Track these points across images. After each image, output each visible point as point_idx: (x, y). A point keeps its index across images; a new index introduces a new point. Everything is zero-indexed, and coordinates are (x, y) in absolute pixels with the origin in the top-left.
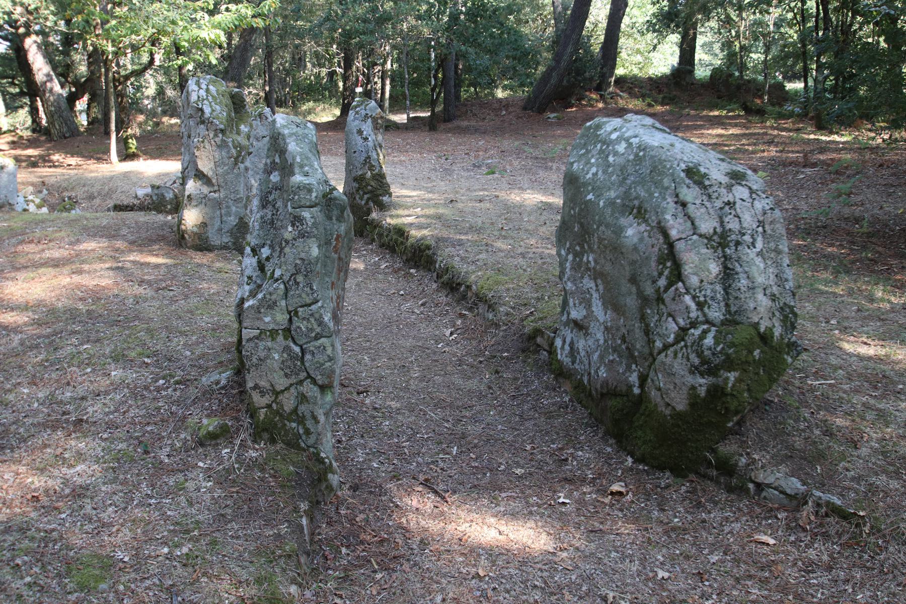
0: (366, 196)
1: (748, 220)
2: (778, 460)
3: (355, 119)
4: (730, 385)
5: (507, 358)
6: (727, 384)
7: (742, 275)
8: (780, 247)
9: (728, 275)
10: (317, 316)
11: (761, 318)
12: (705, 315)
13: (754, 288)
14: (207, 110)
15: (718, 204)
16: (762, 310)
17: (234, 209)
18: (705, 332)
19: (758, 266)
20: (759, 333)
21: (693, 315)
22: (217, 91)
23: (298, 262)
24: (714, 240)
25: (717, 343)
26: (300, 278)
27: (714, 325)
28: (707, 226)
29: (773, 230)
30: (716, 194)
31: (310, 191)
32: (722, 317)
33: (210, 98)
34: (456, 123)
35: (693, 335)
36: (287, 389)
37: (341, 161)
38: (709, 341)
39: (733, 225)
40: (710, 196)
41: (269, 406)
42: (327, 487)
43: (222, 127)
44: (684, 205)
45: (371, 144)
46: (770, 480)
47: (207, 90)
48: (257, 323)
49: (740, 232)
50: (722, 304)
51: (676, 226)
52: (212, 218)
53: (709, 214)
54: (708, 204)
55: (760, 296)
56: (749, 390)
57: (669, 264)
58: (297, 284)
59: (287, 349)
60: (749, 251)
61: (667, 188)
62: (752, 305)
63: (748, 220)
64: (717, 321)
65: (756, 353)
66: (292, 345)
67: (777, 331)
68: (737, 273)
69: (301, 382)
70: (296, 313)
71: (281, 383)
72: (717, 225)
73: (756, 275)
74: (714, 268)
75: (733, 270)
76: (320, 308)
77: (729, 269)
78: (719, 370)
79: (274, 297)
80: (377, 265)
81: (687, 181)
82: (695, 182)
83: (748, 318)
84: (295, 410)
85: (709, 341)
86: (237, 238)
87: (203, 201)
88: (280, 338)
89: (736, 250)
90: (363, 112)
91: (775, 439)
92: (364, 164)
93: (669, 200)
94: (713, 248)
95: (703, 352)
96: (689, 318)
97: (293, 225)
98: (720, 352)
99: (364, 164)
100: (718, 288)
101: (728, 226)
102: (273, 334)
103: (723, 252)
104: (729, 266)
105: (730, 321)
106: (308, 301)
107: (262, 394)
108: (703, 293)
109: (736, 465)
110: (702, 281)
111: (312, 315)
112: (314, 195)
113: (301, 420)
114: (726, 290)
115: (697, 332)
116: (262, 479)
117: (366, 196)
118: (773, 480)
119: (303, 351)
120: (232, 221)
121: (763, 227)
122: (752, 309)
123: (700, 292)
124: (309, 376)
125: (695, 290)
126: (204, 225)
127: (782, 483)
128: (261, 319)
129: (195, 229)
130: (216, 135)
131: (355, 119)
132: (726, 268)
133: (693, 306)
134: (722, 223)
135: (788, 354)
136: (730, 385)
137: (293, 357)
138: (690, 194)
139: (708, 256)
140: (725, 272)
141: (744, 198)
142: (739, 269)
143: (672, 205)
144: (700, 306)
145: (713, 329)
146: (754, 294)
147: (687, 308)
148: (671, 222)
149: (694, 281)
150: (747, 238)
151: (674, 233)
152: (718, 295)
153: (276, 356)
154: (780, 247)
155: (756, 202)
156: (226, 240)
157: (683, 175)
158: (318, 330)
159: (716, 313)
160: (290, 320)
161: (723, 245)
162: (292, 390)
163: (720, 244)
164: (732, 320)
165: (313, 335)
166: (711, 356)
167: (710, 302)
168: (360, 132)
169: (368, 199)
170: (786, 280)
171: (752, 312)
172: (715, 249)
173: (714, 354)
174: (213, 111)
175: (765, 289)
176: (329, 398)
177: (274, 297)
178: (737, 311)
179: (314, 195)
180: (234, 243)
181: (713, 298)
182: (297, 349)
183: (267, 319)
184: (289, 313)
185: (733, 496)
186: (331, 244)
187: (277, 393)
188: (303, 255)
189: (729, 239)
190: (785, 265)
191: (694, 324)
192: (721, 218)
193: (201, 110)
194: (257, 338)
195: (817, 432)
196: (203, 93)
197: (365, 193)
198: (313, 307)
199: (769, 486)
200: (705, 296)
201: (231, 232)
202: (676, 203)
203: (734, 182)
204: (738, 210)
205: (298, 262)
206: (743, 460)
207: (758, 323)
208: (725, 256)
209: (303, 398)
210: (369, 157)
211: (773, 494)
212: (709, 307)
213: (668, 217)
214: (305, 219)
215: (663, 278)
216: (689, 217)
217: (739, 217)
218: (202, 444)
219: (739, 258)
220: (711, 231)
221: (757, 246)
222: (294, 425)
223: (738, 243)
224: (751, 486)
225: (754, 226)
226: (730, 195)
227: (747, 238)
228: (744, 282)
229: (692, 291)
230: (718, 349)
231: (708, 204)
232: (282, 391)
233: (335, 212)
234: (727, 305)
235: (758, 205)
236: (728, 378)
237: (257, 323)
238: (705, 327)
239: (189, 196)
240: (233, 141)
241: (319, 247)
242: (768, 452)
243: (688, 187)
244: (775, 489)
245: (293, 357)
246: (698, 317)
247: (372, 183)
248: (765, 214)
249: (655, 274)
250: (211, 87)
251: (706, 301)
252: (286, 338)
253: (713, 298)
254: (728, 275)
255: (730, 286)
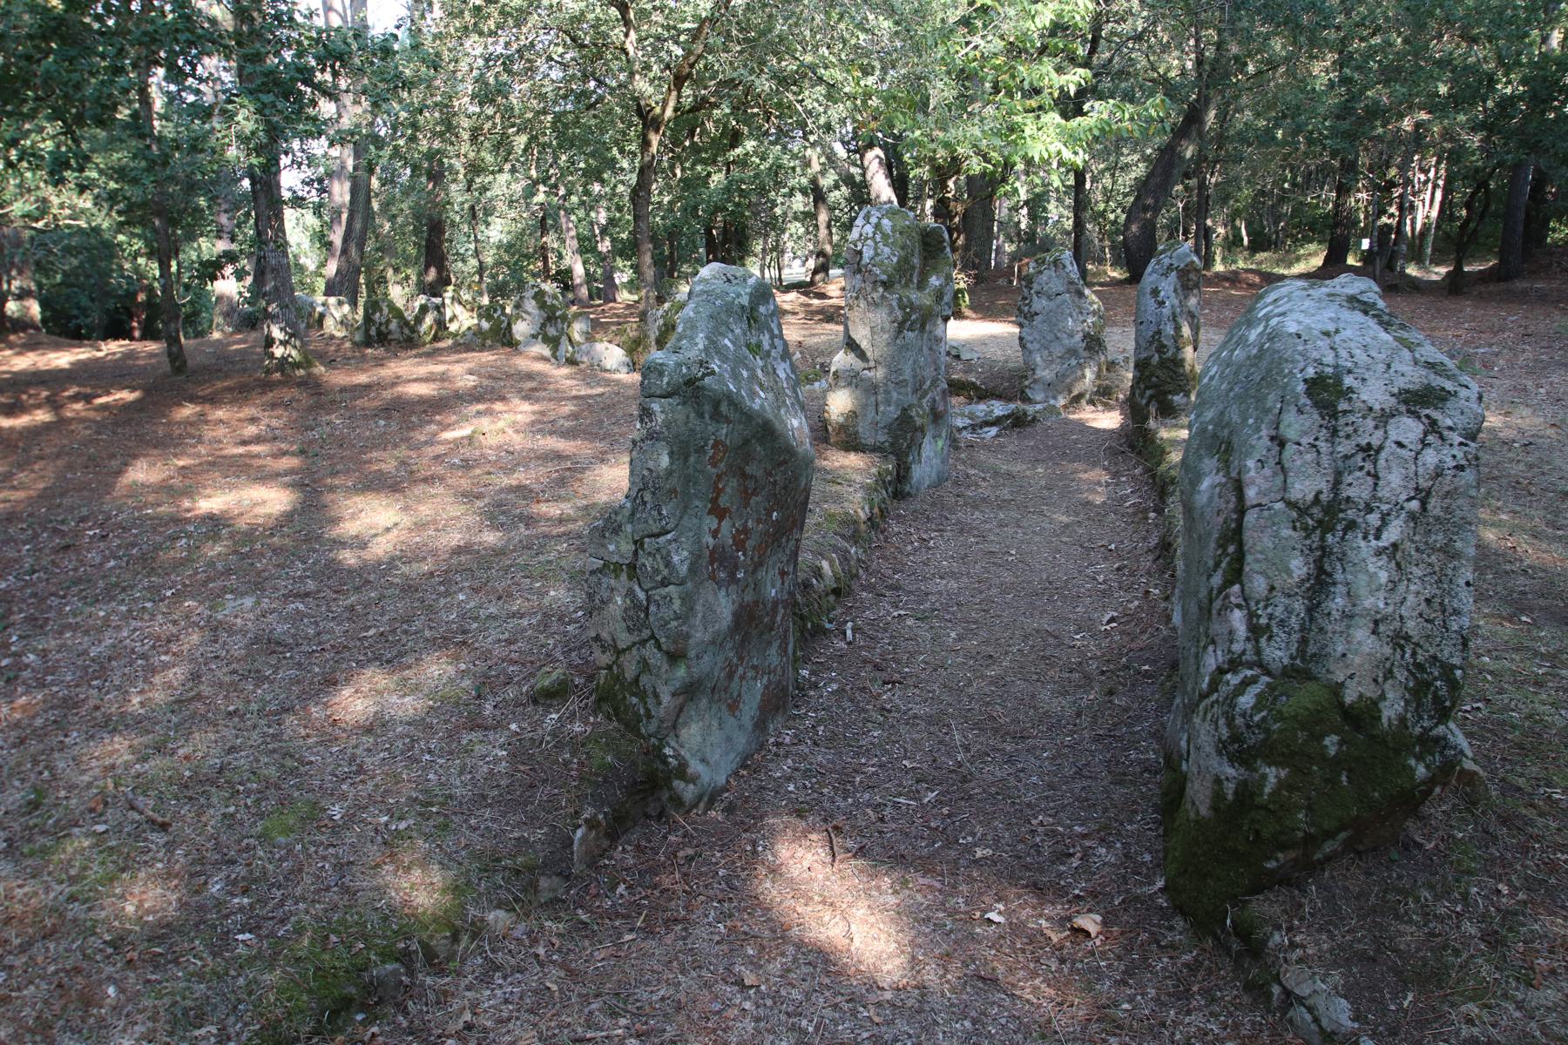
0: (1148, 392)
1: (1394, 481)
2: (1342, 958)
3: (1154, 271)
4: (1267, 790)
5: (1146, 674)
6: (1262, 787)
7: (1341, 589)
8: (1459, 545)
9: (1320, 583)
10: (664, 552)
11: (1351, 677)
12: (1258, 652)
13: (1351, 617)
14: (868, 253)
15: (1345, 447)
16: (1357, 660)
17: (895, 395)
18: (1246, 683)
19: (1373, 576)
20: (1341, 704)
21: (1237, 648)
22: (893, 227)
23: (646, 473)
24: (1311, 516)
25: (1257, 707)
26: (648, 497)
27: (1268, 673)
28: (1304, 487)
29: (1447, 510)
30: (1350, 429)
31: (661, 374)
32: (1286, 661)
33: (878, 238)
34: (1520, 285)
35: (1228, 683)
36: (629, 648)
37: (1131, 331)
38: (1246, 700)
39: (1357, 488)
40: (1334, 432)
41: (609, 668)
42: (671, 798)
43: (884, 277)
44: (1281, 443)
45: (1166, 311)
46: (1304, 990)
47: (878, 226)
48: (602, 552)
49: (1367, 505)
50: (1295, 637)
51: (1258, 481)
52: (865, 406)
53: (1318, 464)
54: (1323, 446)
55: (1361, 634)
56: (1309, 808)
57: (1231, 549)
58: (645, 503)
59: (630, 593)
60: (1363, 544)
61: (1268, 411)
62: (1340, 649)
63: (1394, 481)
64: (1275, 667)
65: (1331, 742)
66: (637, 588)
67: (1392, 709)
68: (1334, 584)
69: (643, 642)
70: (642, 544)
71: (624, 639)
72: (1324, 486)
73: (1363, 592)
74: (1299, 567)
75: (1330, 575)
76: (669, 542)
77: (1325, 572)
78: (1255, 757)
79: (619, 518)
80: (1124, 499)
81: (1304, 400)
82: (1316, 405)
83: (1328, 671)
84: (636, 680)
85: (1246, 700)
86: (896, 437)
87: (851, 379)
88: (624, 577)
89: (1343, 538)
90: (1167, 261)
91: (1361, 917)
92: (1151, 343)
93: (1264, 433)
94: (1305, 529)
95: (1233, 719)
96: (1230, 651)
97: (642, 421)
98: (1258, 726)
99: (1151, 343)
100: (1299, 606)
101: (1351, 492)
102: (617, 569)
103: (1322, 539)
104: (1327, 568)
105: (1297, 671)
106: (656, 531)
107: (604, 649)
108: (1269, 610)
109: (1264, 942)
110: (1272, 588)
111: (658, 550)
112: (666, 380)
113: (642, 695)
114: (1310, 610)
115: (1233, 679)
116: (566, 763)
117: (1148, 392)
118: (1308, 992)
119: (648, 598)
120: (893, 412)
121: (1424, 504)
122: (1338, 655)
123: (1266, 607)
124: (653, 637)
125: (1257, 603)
126: (853, 415)
127: (1320, 1002)
128: (604, 546)
129: (841, 420)
130: (875, 289)
131: (1154, 271)
132: (1321, 570)
133: (1241, 629)
134: (1336, 484)
135: (1419, 758)
136: (1267, 790)
137: (636, 605)
138: (1299, 424)
139: (1292, 543)
140: (1317, 577)
141: (1405, 442)
142: (1339, 576)
143: (1266, 441)
144: (1256, 631)
145: (1266, 679)
146: (1349, 627)
147: (1231, 632)
148: (1252, 473)
149: (1259, 585)
150: (1374, 519)
151: (1251, 493)
152: (1293, 619)
153: (619, 600)
154: (1459, 545)
155: (1429, 452)
156: (882, 439)
157: (1301, 387)
158: (665, 572)
159: (1277, 653)
160: (636, 553)
161: (1325, 527)
162: (634, 651)
163: (1320, 522)
164: (1300, 671)
165: (659, 578)
166: (1243, 729)
167: (1275, 630)
168: (1155, 292)
169: (1151, 397)
170: (1457, 612)
171: (1337, 661)
172: (1308, 532)
173: (1248, 726)
174: (877, 254)
175: (1376, 623)
176: (681, 672)
177: (619, 518)
178: (1314, 655)
179: (666, 380)
180: (892, 445)
181: (1282, 624)
182: (641, 595)
183: (612, 548)
184: (635, 542)
185: (1246, 999)
186: (705, 453)
187: (619, 652)
188: (651, 464)
189: (1341, 515)
190: (1462, 582)
191: (1234, 664)
192: (1338, 475)
193: (860, 253)
194: (600, 571)
195: (1470, 928)
196: (869, 229)
197: (1147, 388)
198: (662, 539)
199: (1301, 1000)
200: (1271, 617)
201: (889, 427)
202: (1272, 439)
203: (1403, 408)
204: (1382, 463)
205: (646, 473)
206: (1277, 937)
207: (1342, 685)
208: (1322, 548)
209: (644, 665)
210: (1159, 332)
211: (1303, 1019)
212: (1270, 638)
213: (1251, 463)
214: (654, 413)
215: (1220, 572)
216: (1283, 468)
217: (1376, 477)
218: (535, 702)
219: (1344, 554)
220: (1310, 497)
221: (1384, 536)
222: (634, 700)
223: (1351, 525)
224: (1276, 990)
225: (1403, 497)
226: (1379, 433)
227: (1374, 519)
228: (1338, 602)
229: (1252, 604)
230: (1257, 718)
231: (1323, 446)
232: (624, 650)
233: (707, 408)
234: (1304, 642)
235: (1430, 458)
236: (1264, 777)
237: (602, 552)
238: (1249, 673)
239: (835, 373)
240: (900, 299)
241: (671, 454)
242: (1332, 937)
243: (1300, 412)
244: (1310, 1010)
245: (636, 605)
246: (1244, 652)
247: (1159, 372)
248: (1438, 475)
249: (1211, 563)
250: (885, 222)
251: (1268, 625)
252: (630, 579)
253: (1282, 624)
254: (1320, 583)
255: (1319, 603)
